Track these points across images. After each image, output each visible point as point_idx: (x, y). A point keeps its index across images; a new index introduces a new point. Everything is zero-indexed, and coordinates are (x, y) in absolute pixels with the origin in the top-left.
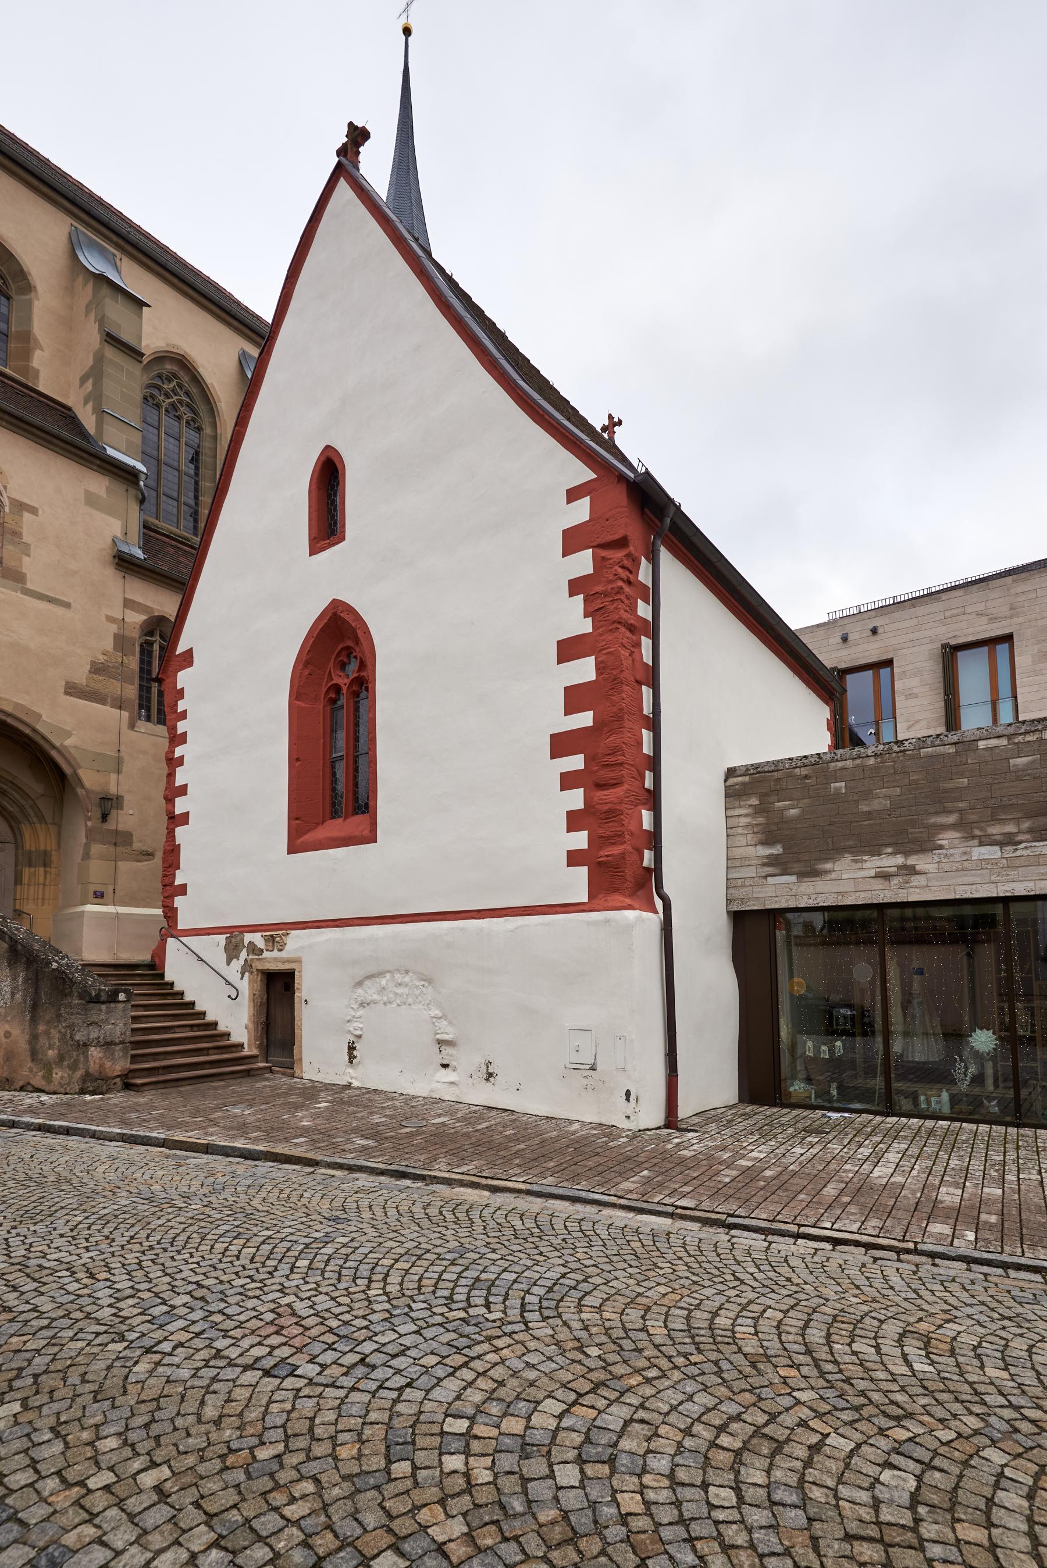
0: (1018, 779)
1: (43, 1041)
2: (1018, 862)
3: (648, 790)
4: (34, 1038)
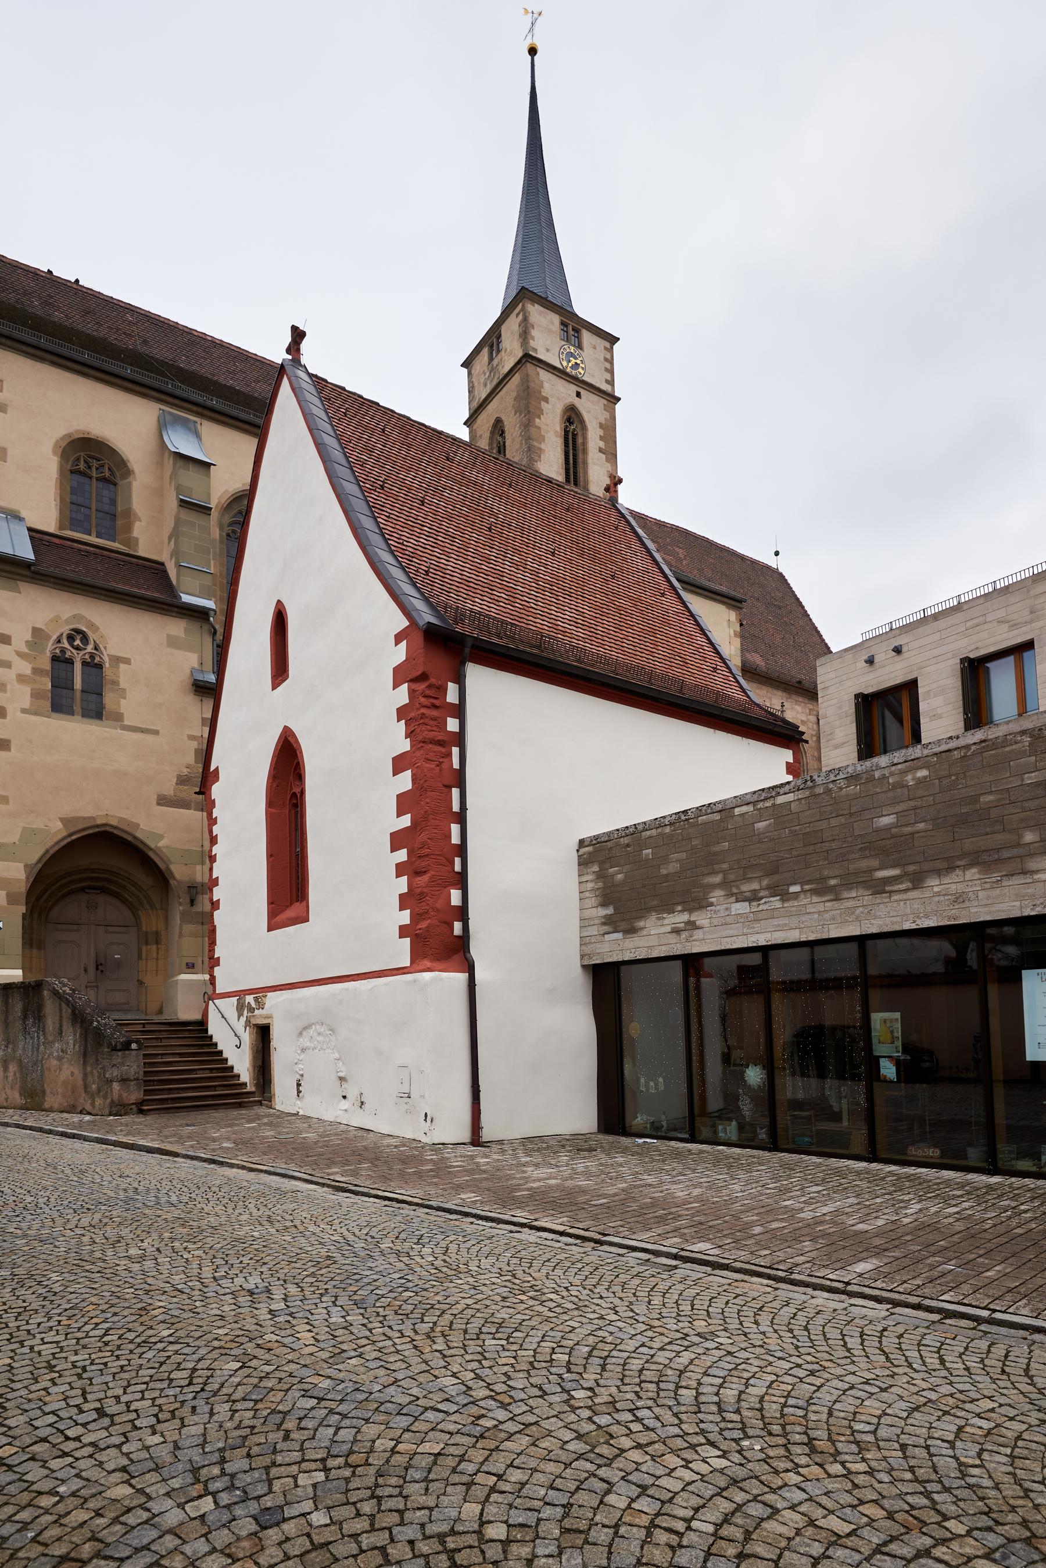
0: (760, 842)
1: (90, 1078)
2: (760, 916)
3: (458, 873)
4: (85, 1076)
